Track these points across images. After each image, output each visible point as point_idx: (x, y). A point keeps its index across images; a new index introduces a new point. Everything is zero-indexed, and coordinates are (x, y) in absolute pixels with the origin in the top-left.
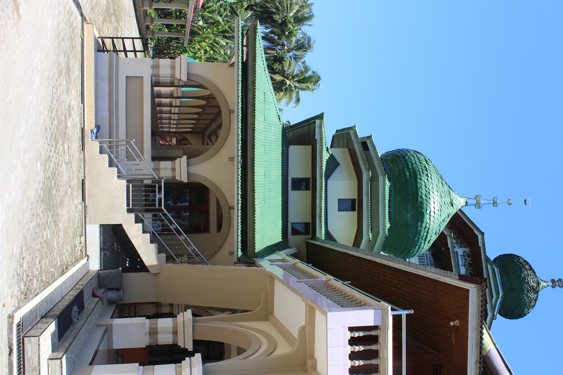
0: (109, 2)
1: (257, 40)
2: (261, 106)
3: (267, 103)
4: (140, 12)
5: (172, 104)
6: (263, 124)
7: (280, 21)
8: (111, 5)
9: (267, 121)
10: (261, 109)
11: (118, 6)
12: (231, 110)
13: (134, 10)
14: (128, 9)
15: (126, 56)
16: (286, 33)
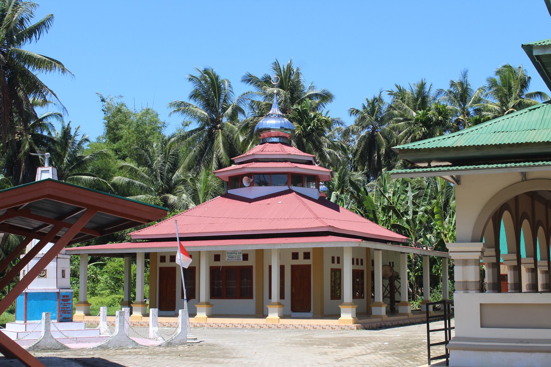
0: (391, 353)
1: (418, 147)
2: (513, 136)
3: (509, 127)
4: (414, 319)
5: (532, 269)
6: (540, 131)
7: (423, 129)
8: (396, 351)
9: (536, 126)
10: (517, 135)
11: (400, 344)
12: (522, 179)
13: (412, 326)
14: (408, 333)
15: (453, 328)
16: (440, 119)
